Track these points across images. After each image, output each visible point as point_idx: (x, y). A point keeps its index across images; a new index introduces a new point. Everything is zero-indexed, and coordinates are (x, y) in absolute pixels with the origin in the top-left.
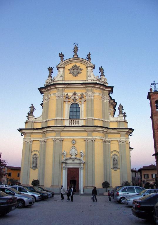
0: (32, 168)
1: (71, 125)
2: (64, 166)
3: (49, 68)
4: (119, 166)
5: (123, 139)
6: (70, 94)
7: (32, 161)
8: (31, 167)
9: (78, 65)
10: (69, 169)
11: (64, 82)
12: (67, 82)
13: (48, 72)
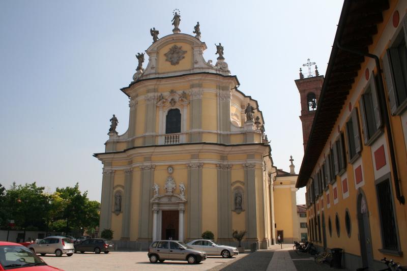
0: (114, 212)
1: (166, 144)
2: (155, 207)
3: (138, 55)
4: (244, 206)
5: (148, 164)
6: (166, 94)
7: (114, 203)
8: (113, 210)
9: (179, 45)
11: (157, 76)
12: (161, 76)
13: (137, 61)
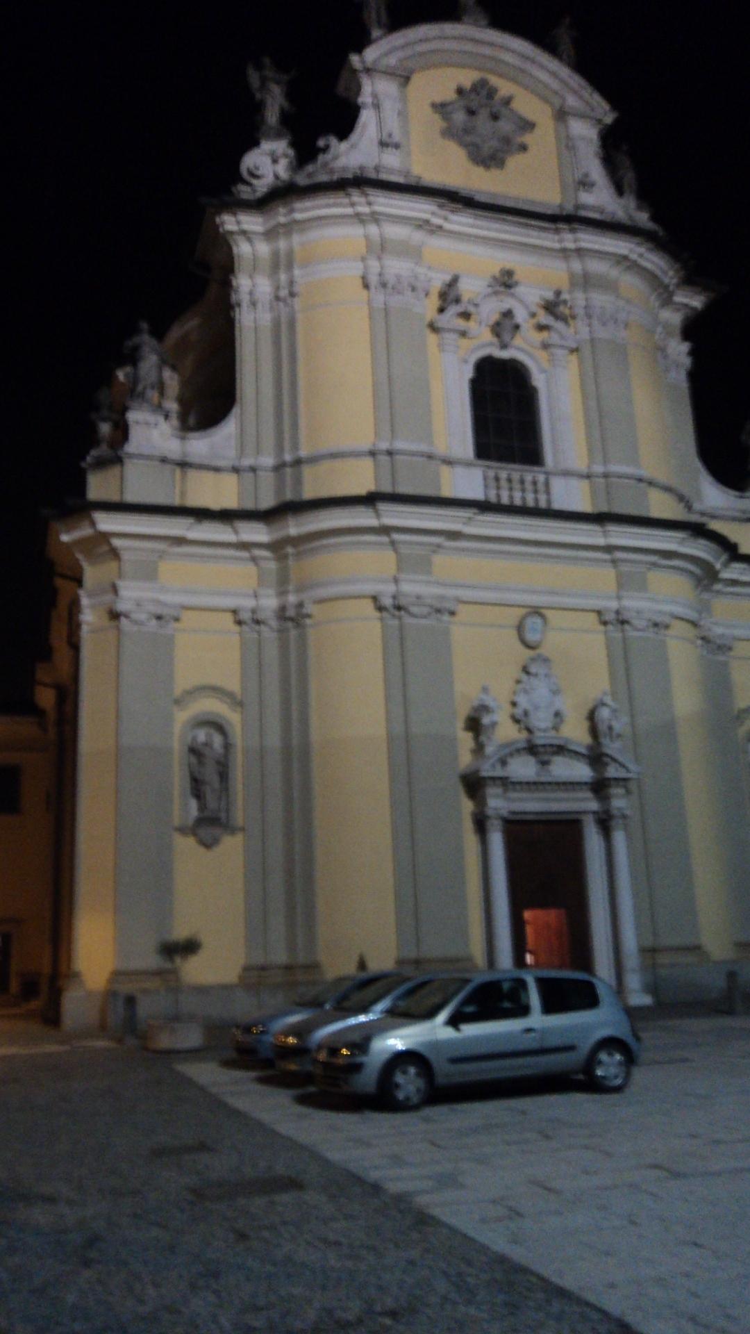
10: (517, 829)
